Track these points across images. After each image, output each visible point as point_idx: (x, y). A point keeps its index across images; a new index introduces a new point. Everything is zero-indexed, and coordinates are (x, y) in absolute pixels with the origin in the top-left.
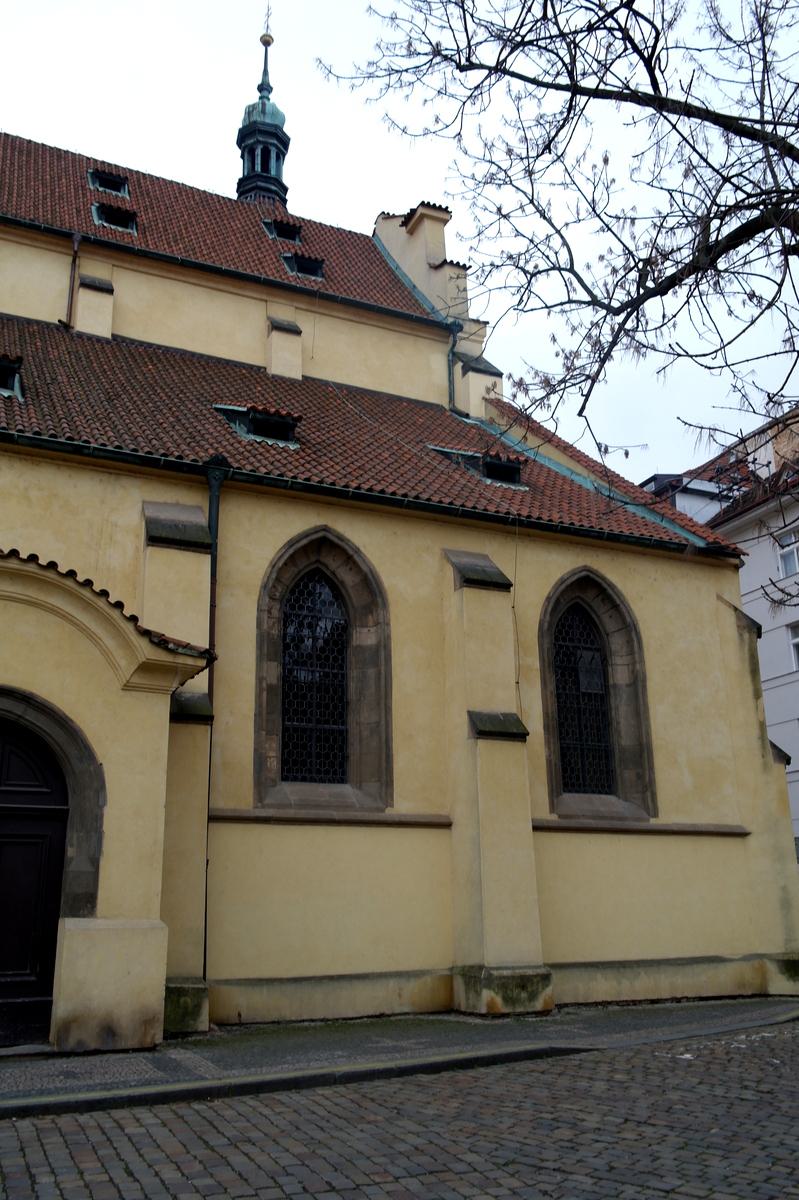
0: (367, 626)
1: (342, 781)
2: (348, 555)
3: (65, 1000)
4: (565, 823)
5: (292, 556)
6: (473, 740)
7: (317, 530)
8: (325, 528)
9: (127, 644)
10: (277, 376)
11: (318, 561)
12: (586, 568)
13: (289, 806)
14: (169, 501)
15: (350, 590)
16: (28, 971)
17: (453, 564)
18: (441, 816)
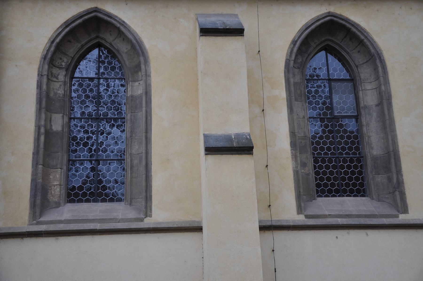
0: (138, 81)
4: (311, 222)
7: (88, 12)
8: (96, 10)
11: (97, 37)
12: (329, 14)
18: (194, 221)
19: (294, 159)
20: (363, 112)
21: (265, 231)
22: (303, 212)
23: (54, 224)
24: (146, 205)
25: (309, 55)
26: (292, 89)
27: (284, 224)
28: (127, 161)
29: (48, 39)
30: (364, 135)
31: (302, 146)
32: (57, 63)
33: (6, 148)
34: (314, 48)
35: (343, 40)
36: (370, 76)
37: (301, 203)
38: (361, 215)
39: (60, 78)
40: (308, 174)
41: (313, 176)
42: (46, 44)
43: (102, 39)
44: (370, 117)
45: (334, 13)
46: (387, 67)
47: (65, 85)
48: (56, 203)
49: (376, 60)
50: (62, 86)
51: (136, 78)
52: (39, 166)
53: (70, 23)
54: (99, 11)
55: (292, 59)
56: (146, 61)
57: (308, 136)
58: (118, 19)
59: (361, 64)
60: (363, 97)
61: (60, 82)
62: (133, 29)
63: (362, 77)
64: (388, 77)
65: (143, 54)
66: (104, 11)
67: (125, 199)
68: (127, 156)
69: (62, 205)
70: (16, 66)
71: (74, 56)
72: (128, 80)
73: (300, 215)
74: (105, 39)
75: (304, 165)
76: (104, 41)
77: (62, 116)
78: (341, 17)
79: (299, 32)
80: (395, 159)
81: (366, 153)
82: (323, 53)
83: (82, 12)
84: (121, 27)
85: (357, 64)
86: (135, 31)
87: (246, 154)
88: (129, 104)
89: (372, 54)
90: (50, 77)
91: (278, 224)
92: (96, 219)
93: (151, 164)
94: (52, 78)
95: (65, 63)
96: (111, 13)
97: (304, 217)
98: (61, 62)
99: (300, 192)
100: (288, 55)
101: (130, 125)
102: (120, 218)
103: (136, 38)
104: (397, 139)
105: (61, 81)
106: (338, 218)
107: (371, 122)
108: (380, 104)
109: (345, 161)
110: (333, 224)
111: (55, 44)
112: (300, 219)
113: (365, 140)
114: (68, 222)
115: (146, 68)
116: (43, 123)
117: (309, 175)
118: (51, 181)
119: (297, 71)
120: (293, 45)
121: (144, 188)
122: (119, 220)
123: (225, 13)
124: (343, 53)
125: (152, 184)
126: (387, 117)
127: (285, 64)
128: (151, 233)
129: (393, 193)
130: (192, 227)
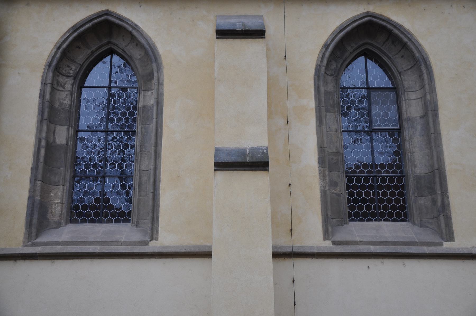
0: (151, 90)
7: (99, 15)
8: (107, 13)
11: (109, 43)
12: (368, 14)
19: (322, 177)
20: (405, 125)
21: (286, 259)
22: (331, 238)
23: (51, 246)
24: (153, 227)
25: (344, 61)
26: (323, 98)
27: (307, 251)
28: (136, 178)
29: (54, 45)
30: (406, 151)
31: (333, 163)
32: (64, 71)
33: (4, 162)
34: (351, 53)
35: (384, 43)
36: (415, 84)
37: (328, 227)
38: (398, 242)
39: (66, 87)
40: (339, 195)
41: (345, 198)
42: (52, 50)
43: (114, 44)
44: (414, 131)
45: (373, 13)
46: (434, 74)
47: (72, 95)
48: (56, 222)
49: (421, 66)
50: (69, 95)
51: (149, 86)
52: (38, 182)
53: (78, 27)
54: (110, 14)
55: (323, 65)
56: (159, 68)
57: (341, 151)
58: (131, 22)
59: (404, 71)
60: (406, 107)
61: (66, 91)
62: (146, 33)
63: (406, 85)
64: (434, 85)
65: (155, 61)
66: (115, 14)
67: (132, 220)
68: (135, 172)
69: (63, 226)
71: (84, 63)
72: (140, 89)
73: (326, 241)
74: (117, 45)
75: (334, 184)
76: (116, 47)
77: (67, 128)
78: (381, 18)
79: (332, 34)
80: (440, 178)
81: (408, 172)
82: (362, 59)
83: (92, 15)
84: (133, 31)
85: (400, 70)
86: (148, 35)
87: (261, 170)
88: (141, 115)
89: (416, 59)
90: (55, 86)
91: (299, 251)
92: (97, 241)
93: (160, 181)
94: (59, 87)
95: (73, 70)
96: (122, 16)
97: (331, 243)
98: (69, 70)
99: (327, 215)
100: (319, 60)
101: (140, 138)
102: (122, 241)
103: (149, 43)
104: (444, 156)
105: (68, 90)
106: (371, 245)
107: (415, 136)
108: (425, 116)
109: (383, 180)
110: (365, 252)
111: (61, 50)
112: (326, 246)
113: (407, 156)
114: (66, 243)
115: (158, 76)
116: (44, 135)
117: (341, 196)
118: (52, 199)
119: (330, 78)
120: (325, 49)
121: (150, 208)
122: (121, 242)
123: (249, 14)
124: (385, 58)
125: (160, 204)
126: (432, 130)
127: (315, 70)
128: (156, 258)
129: (438, 217)
130: (202, 252)
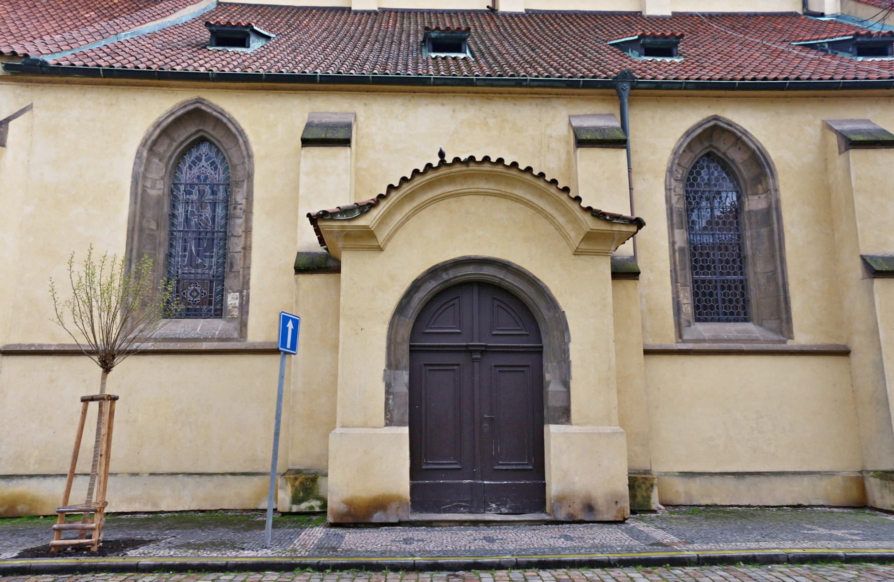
0: (757, 194)
1: (746, 320)
2: (738, 138)
3: (554, 486)
5: (689, 145)
6: (869, 280)
7: (708, 120)
8: (716, 118)
9: (574, 220)
10: (652, 16)
11: (710, 146)
13: (704, 341)
14: (589, 113)
15: (741, 167)
16: (526, 462)
17: (836, 132)
43: (715, 148)
70: (644, 179)
